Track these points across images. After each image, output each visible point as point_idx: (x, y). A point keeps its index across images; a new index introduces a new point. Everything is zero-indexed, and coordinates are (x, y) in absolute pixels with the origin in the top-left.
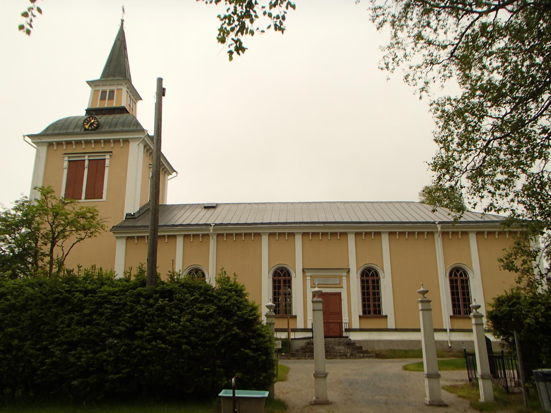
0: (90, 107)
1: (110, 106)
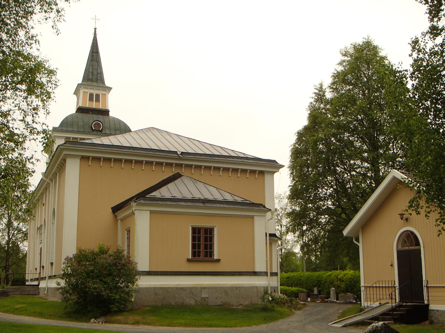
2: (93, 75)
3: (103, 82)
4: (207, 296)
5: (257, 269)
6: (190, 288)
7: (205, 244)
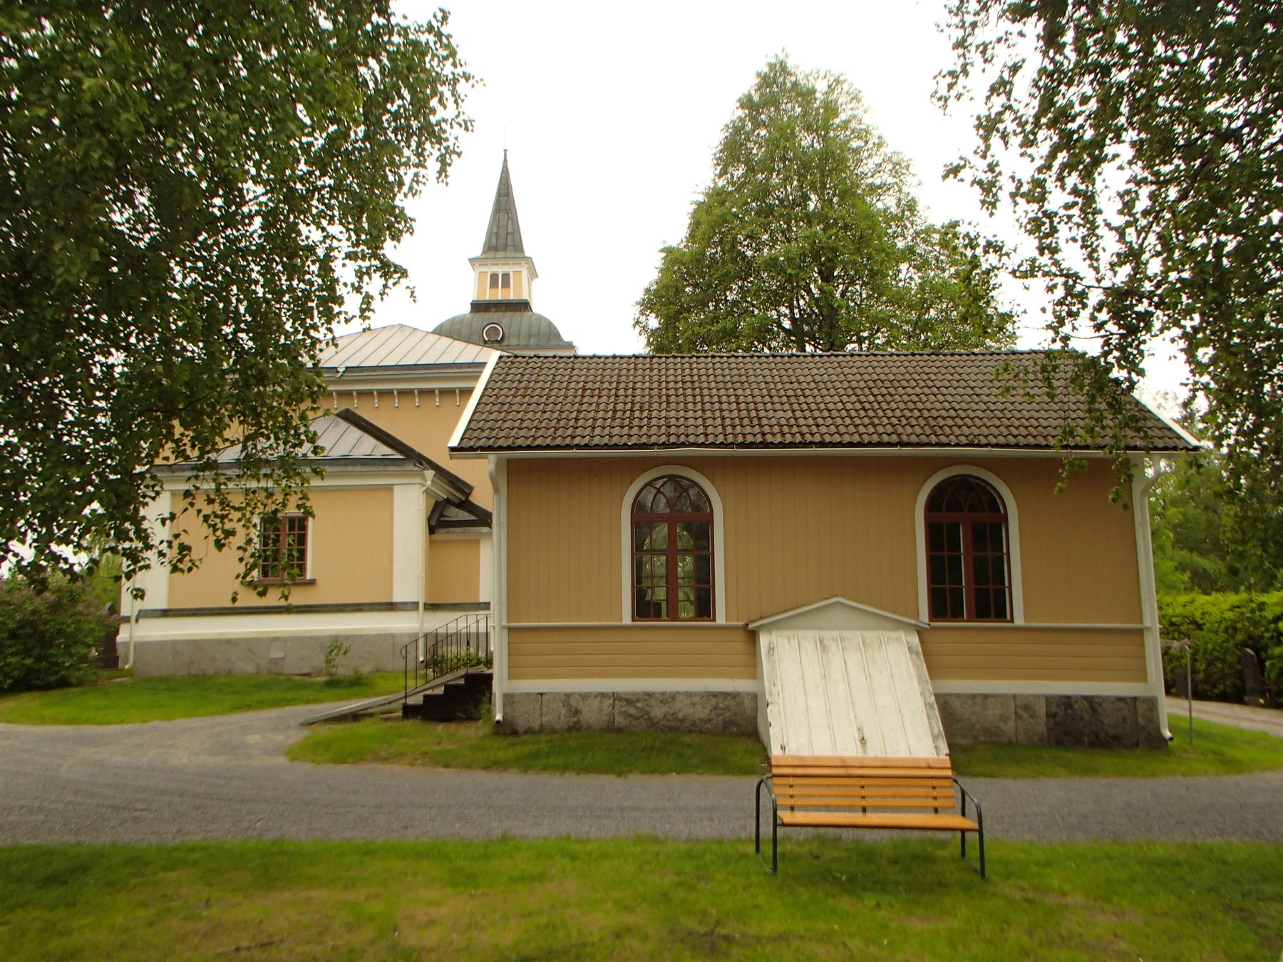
3: (519, 248)
4: (281, 655)
5: (397, 599)
7: (977, 591)
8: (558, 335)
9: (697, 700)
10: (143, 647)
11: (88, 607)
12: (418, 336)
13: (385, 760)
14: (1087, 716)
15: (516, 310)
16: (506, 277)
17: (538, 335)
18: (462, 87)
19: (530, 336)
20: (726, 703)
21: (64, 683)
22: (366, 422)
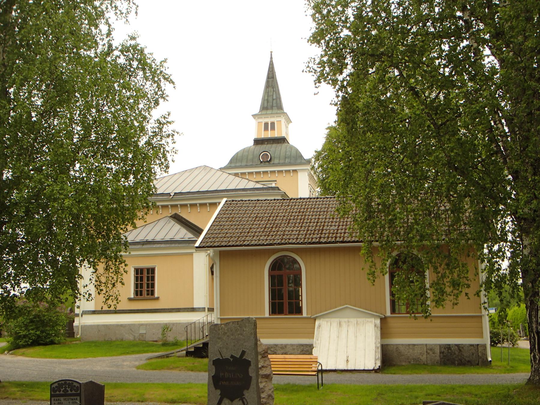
0: (256, 137)
1: (273, 136)
2: (268, 102)
3: (280, 107)
4: (144, 332)
5: (195, 306)
6: (129, 325)
8: (301, 156)
9: (295, 347)
10: (84, 328)
11: (61, 309)
12: (213, 172)
13: (171, 369)
14: (457, 353)
15: (278, 143)
16: (273, 124)
17: (290, 157)
18: (176, 137)
19: (286, 158)
20: (307, 349)
21: (52, 343)
22: (185, 219)
